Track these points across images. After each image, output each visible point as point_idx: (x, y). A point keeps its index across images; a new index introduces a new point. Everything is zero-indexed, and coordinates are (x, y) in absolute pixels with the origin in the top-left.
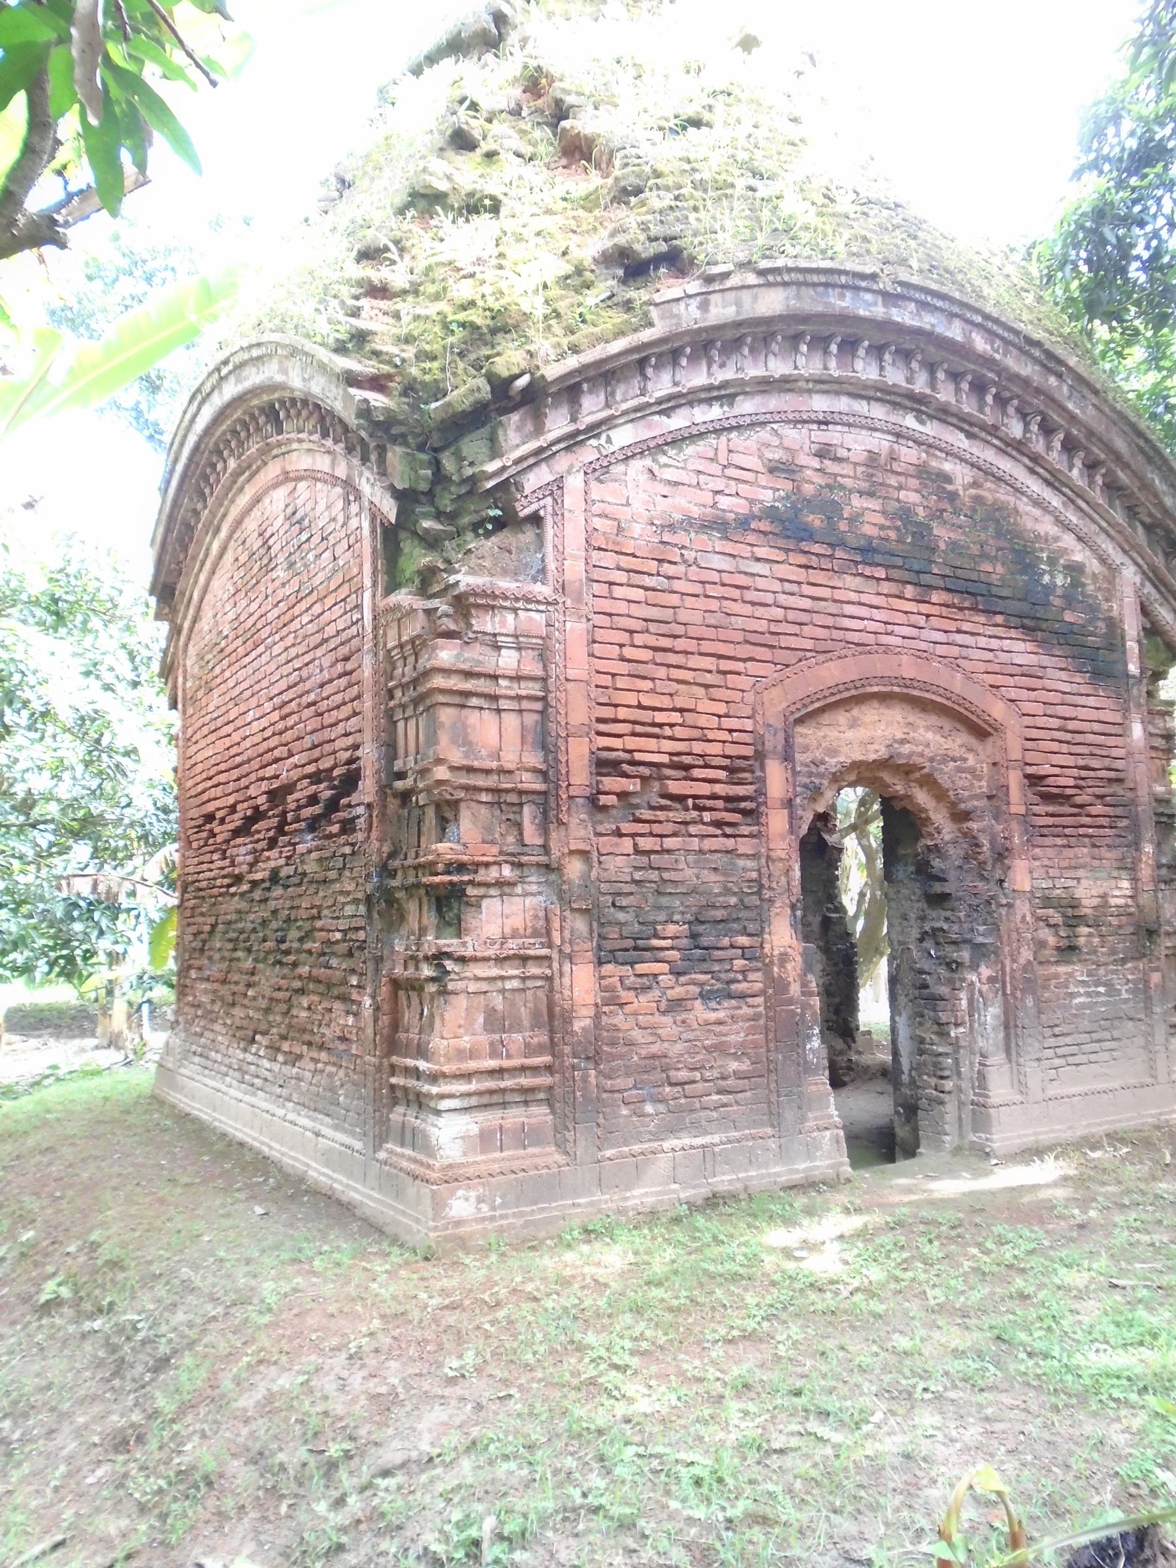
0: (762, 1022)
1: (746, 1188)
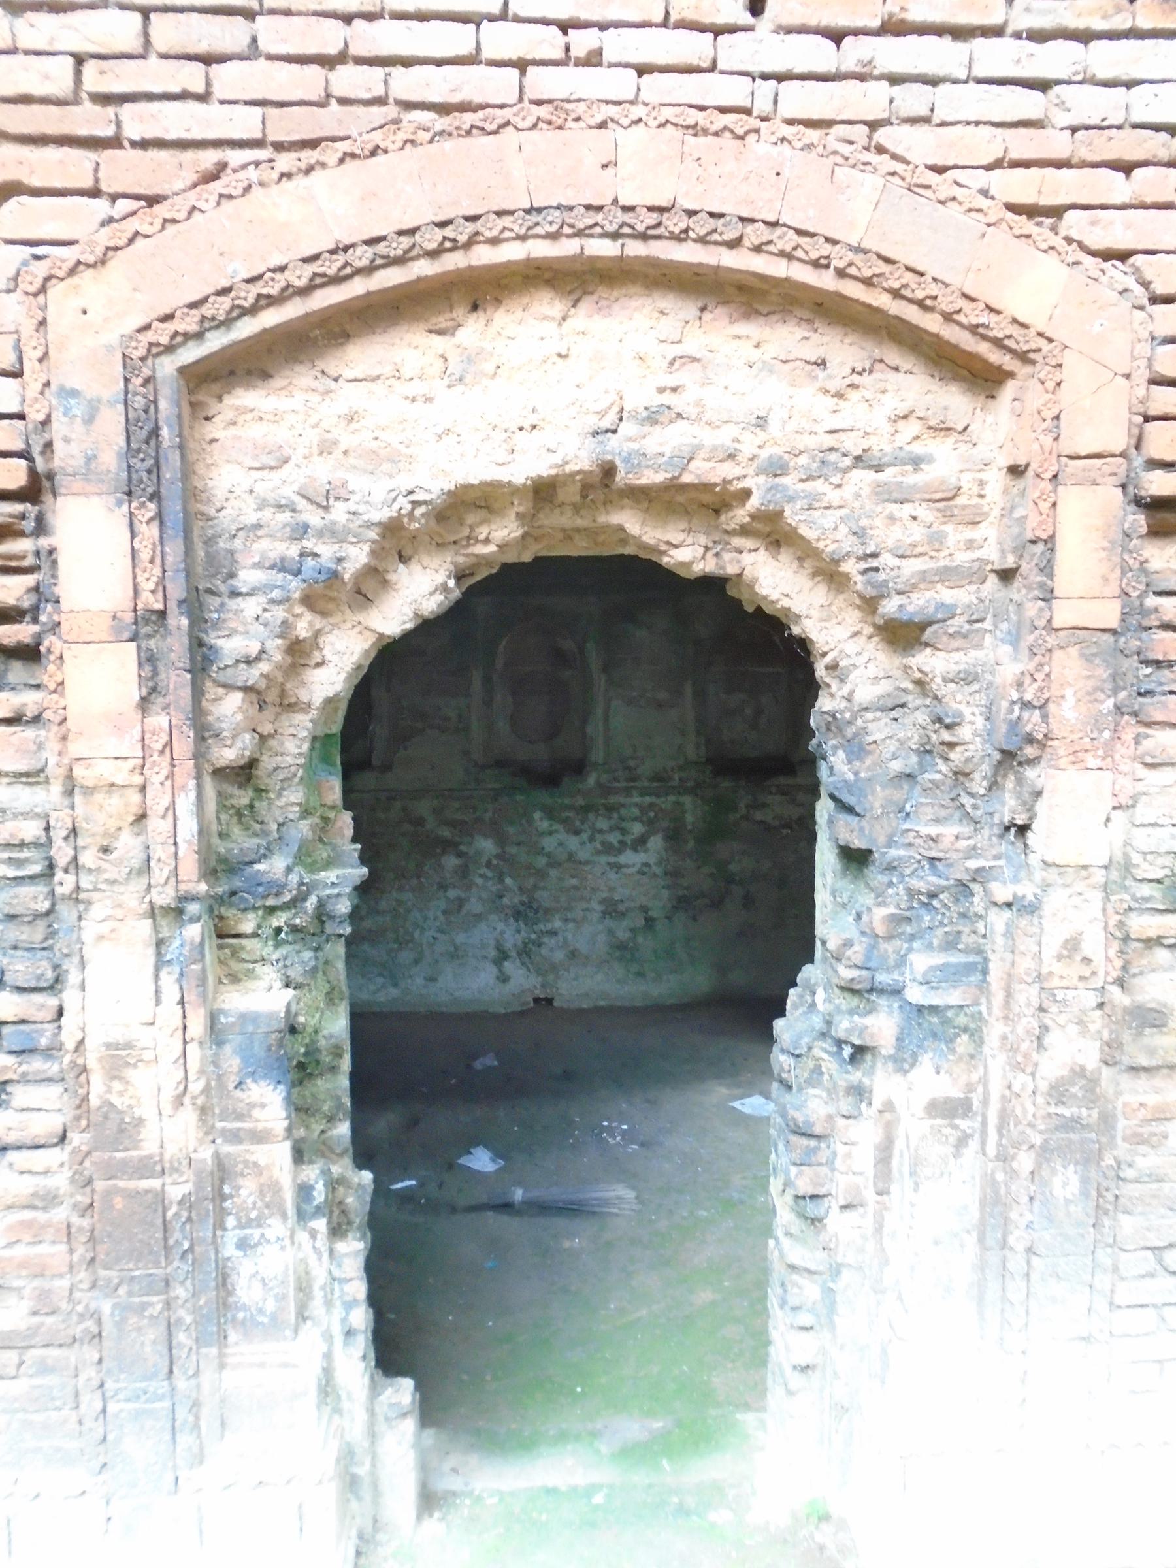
0: (60, 1214)
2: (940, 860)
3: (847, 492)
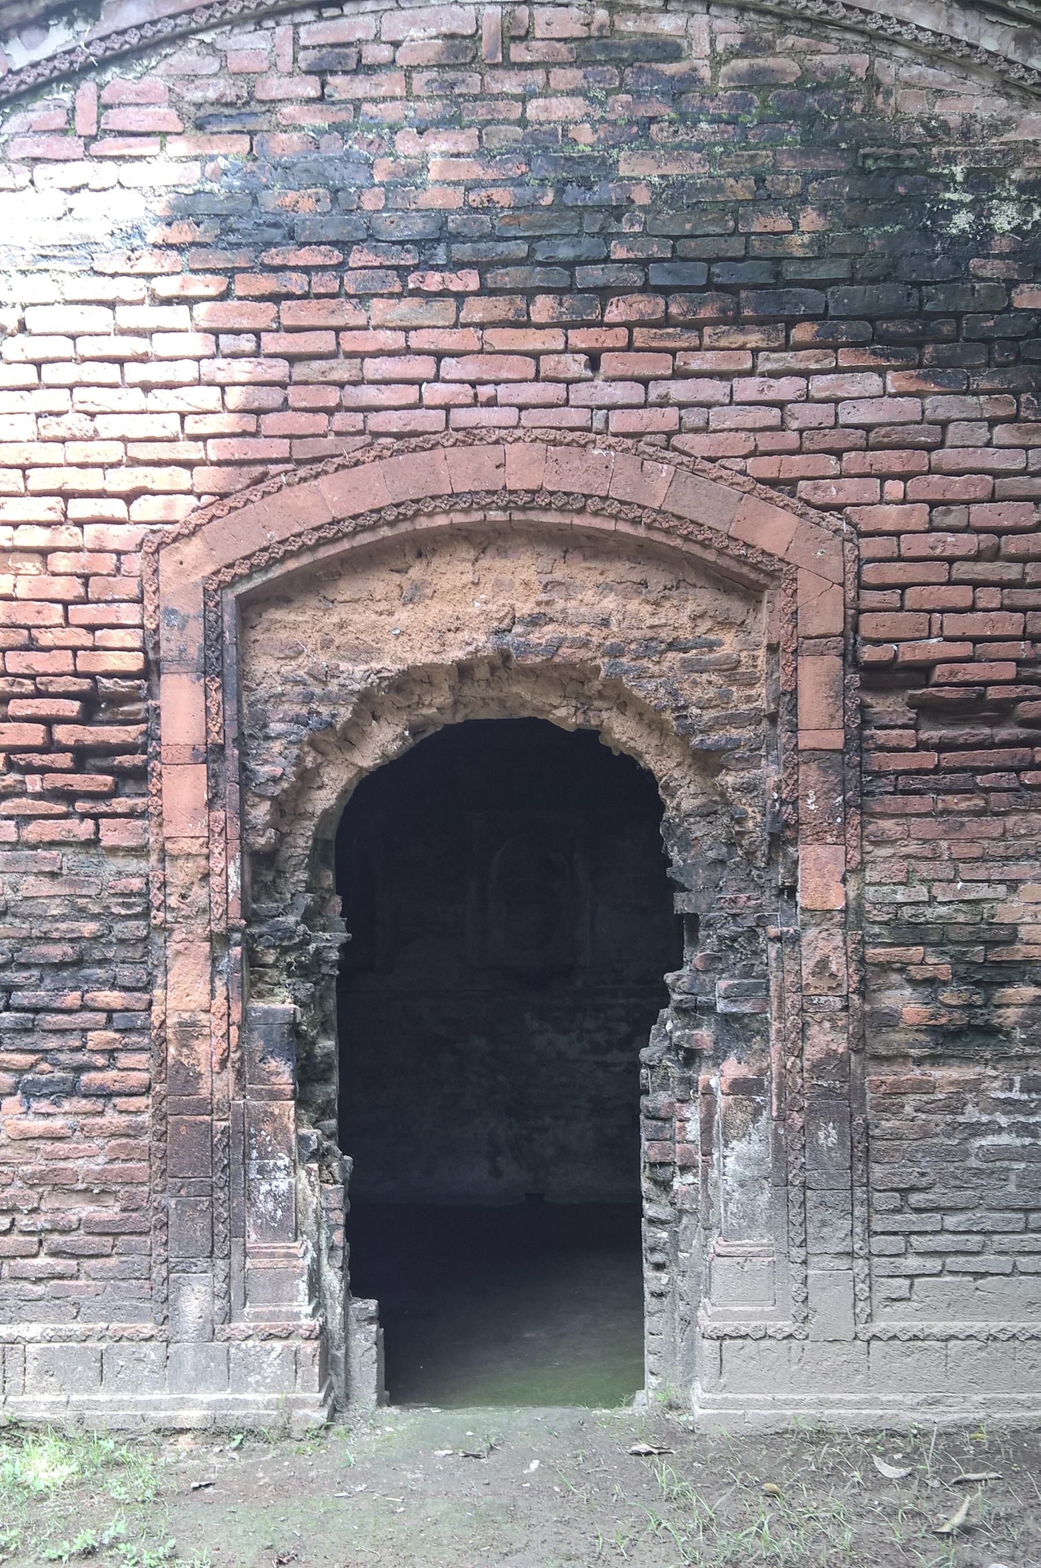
0: (146, 1140)
1: (81, 1421)
2: (738, 915)
3: (665, 666)
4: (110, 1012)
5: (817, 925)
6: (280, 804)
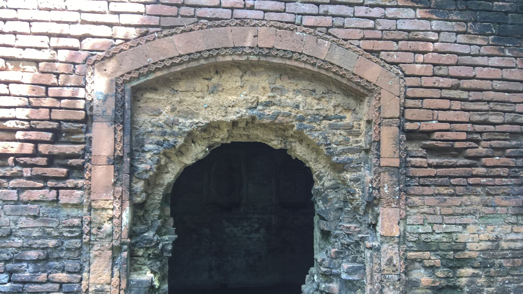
3: (322, 126)
4: (61, 284)
5: (387, 243)
6: (148, 181)
